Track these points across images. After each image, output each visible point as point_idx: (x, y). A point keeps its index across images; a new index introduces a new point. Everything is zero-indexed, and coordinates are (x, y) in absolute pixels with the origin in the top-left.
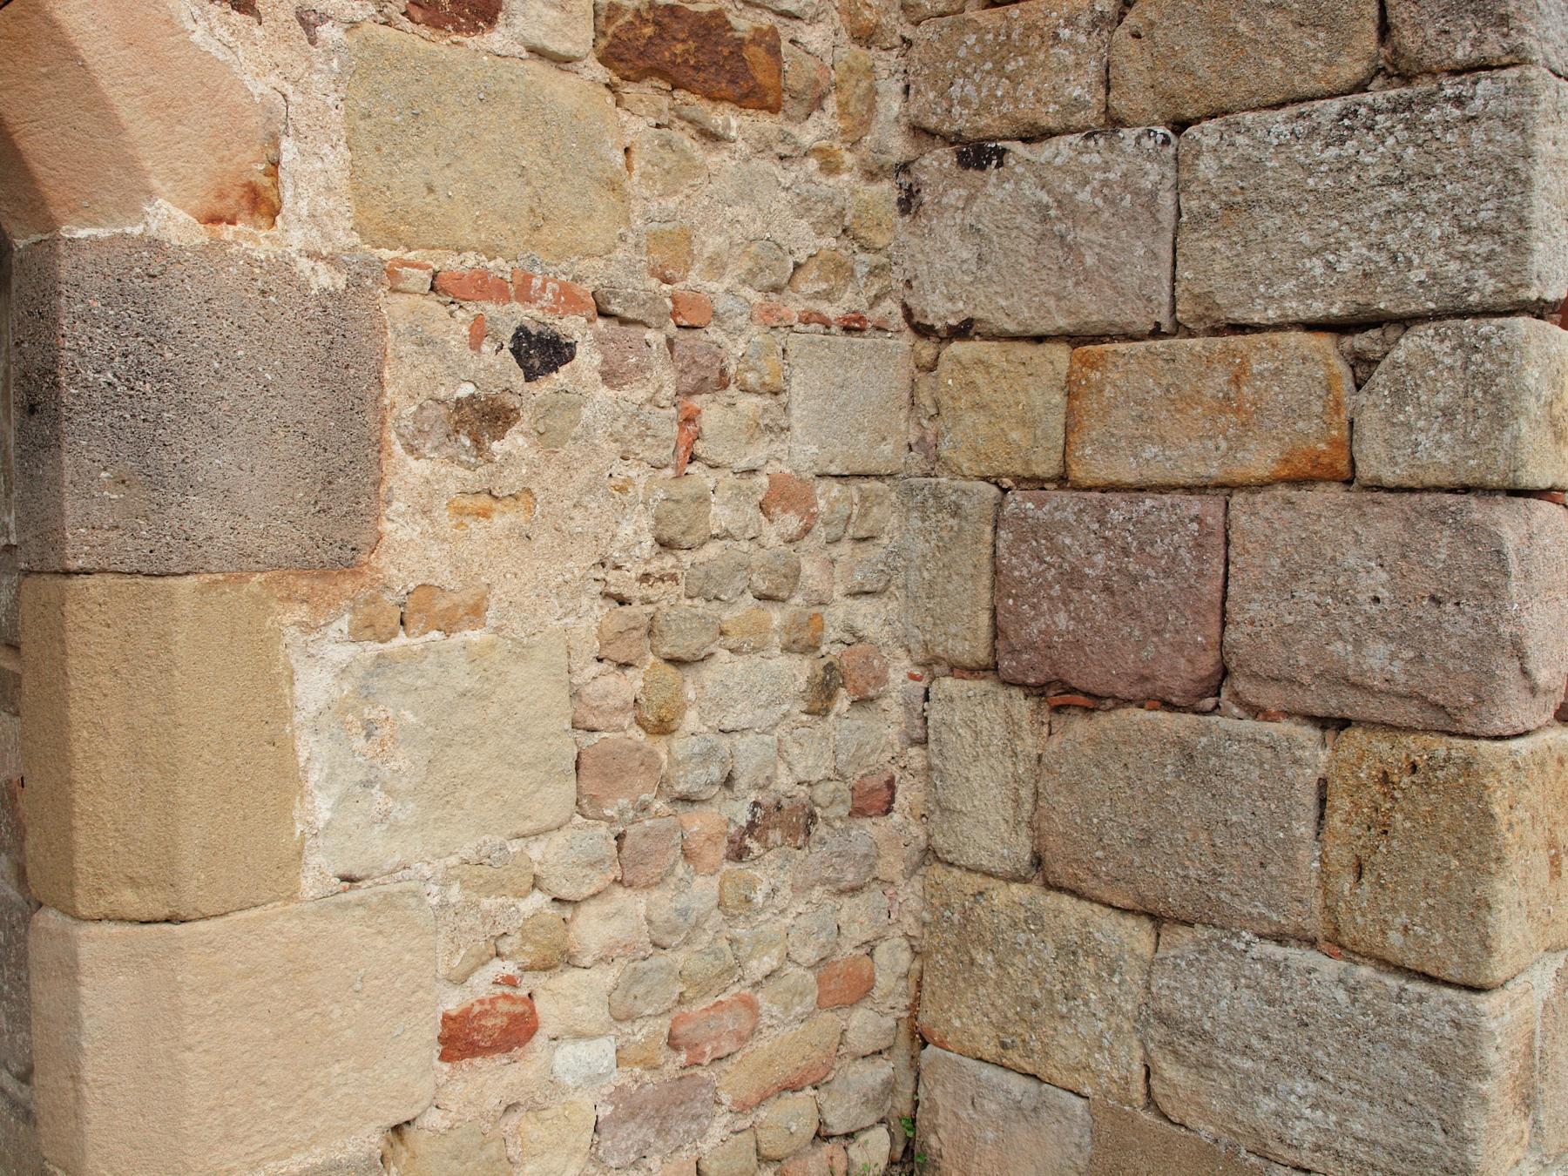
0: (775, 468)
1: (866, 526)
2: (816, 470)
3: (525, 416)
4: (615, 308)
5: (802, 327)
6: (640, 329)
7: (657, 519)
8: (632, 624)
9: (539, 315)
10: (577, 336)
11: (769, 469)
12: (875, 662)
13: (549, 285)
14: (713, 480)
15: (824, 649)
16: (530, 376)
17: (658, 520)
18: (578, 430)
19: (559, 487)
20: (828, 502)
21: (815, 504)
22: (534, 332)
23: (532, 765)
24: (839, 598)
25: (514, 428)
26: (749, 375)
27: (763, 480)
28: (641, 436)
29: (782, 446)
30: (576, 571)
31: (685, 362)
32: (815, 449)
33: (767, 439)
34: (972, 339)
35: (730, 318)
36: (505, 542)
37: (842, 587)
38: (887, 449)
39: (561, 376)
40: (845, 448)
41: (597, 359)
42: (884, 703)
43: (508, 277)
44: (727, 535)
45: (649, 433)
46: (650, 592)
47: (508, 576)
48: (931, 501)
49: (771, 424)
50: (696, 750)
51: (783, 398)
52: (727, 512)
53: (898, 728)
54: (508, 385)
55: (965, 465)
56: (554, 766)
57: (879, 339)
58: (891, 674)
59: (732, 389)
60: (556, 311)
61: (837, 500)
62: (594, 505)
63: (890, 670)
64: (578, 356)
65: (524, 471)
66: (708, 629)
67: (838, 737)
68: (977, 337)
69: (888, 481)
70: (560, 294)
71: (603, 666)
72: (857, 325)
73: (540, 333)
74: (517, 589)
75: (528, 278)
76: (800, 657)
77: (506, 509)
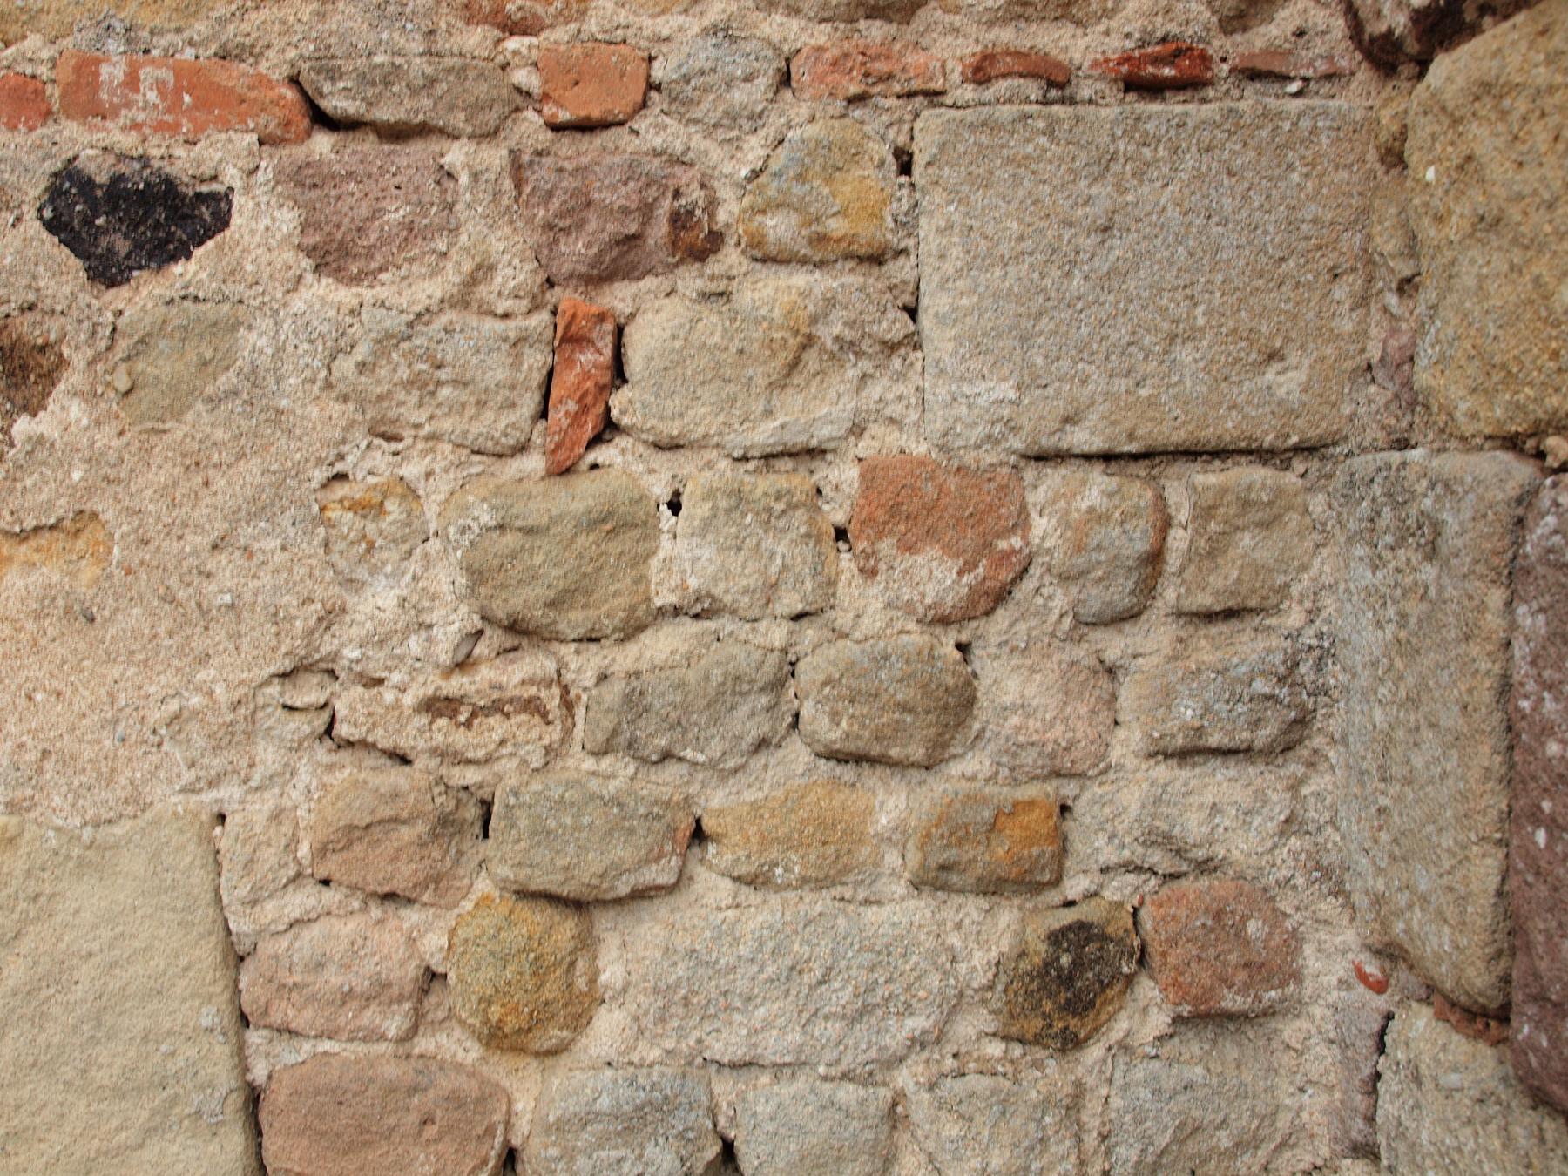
0: (878, 442)
1: (1217, 582)
2: (1017, 443)
3: (78, 358)
4: (336, 103)
5: (968, 93)
6: (434, 145)
7: (470, 570)
8: (386, 812)
9: (127, 141)
10: (231, 176)
11: (865, 447)
12: (1253, 927)
13: (147, 74)
14: (665, 476)
15: (1075, 886)
16: (106, 273)
17: (477, 576)
18: (227, 380)
19: (174, 505)
20: (1065, 522)
21: (1021, 523)
22: (102, 178)
23: (119, 1093)
24: (1130, 762)
25: (61, 387)
26: (770, 221)
27: (843, 475)
28: (424, 386)
29: (900, 388)
30: (219, 690)
31: (555, 204)
32: (1007, 391)
33: (852, 373)
34: (1474, 30)
35: (706, 89)
36: (31, 626)
37: (1136, 735)
38: (1288, 382)
39: (195, 269)
40: (1122, 384)
41: (288, 219)
42: (1291, 1030)
43: (44, 71)
44: (703, 609)
45: (443, 375)
46: (460, 738)
47: (39, 697)
48: (1387, 513)
49: (849, 335)
50: (604, 1103)
51: (900, 270)
52: (707, 553)
53: (1324, 1098)
54: (31, 297)
55: (1463, 407)
56: (174, 1100)
57: (1251, 99)
58: (1310, 959)
59: (730, 258)
60: (174, 128)
61: (1096, 517)
62: (272, 543)
63: (1308, 950)
64: (236, 220)
65: (76, 476)
66: (631, 831)
67: (1116, 1102)
68: (1487, 21)
69: (1299, 465)
70: (178, 91)
71: (330, 896)
72: (1168, 72)
73: (117, 179)
74: (63, 727)
75: (87, 68)
76: (983, 903)
77: (36, 557)
